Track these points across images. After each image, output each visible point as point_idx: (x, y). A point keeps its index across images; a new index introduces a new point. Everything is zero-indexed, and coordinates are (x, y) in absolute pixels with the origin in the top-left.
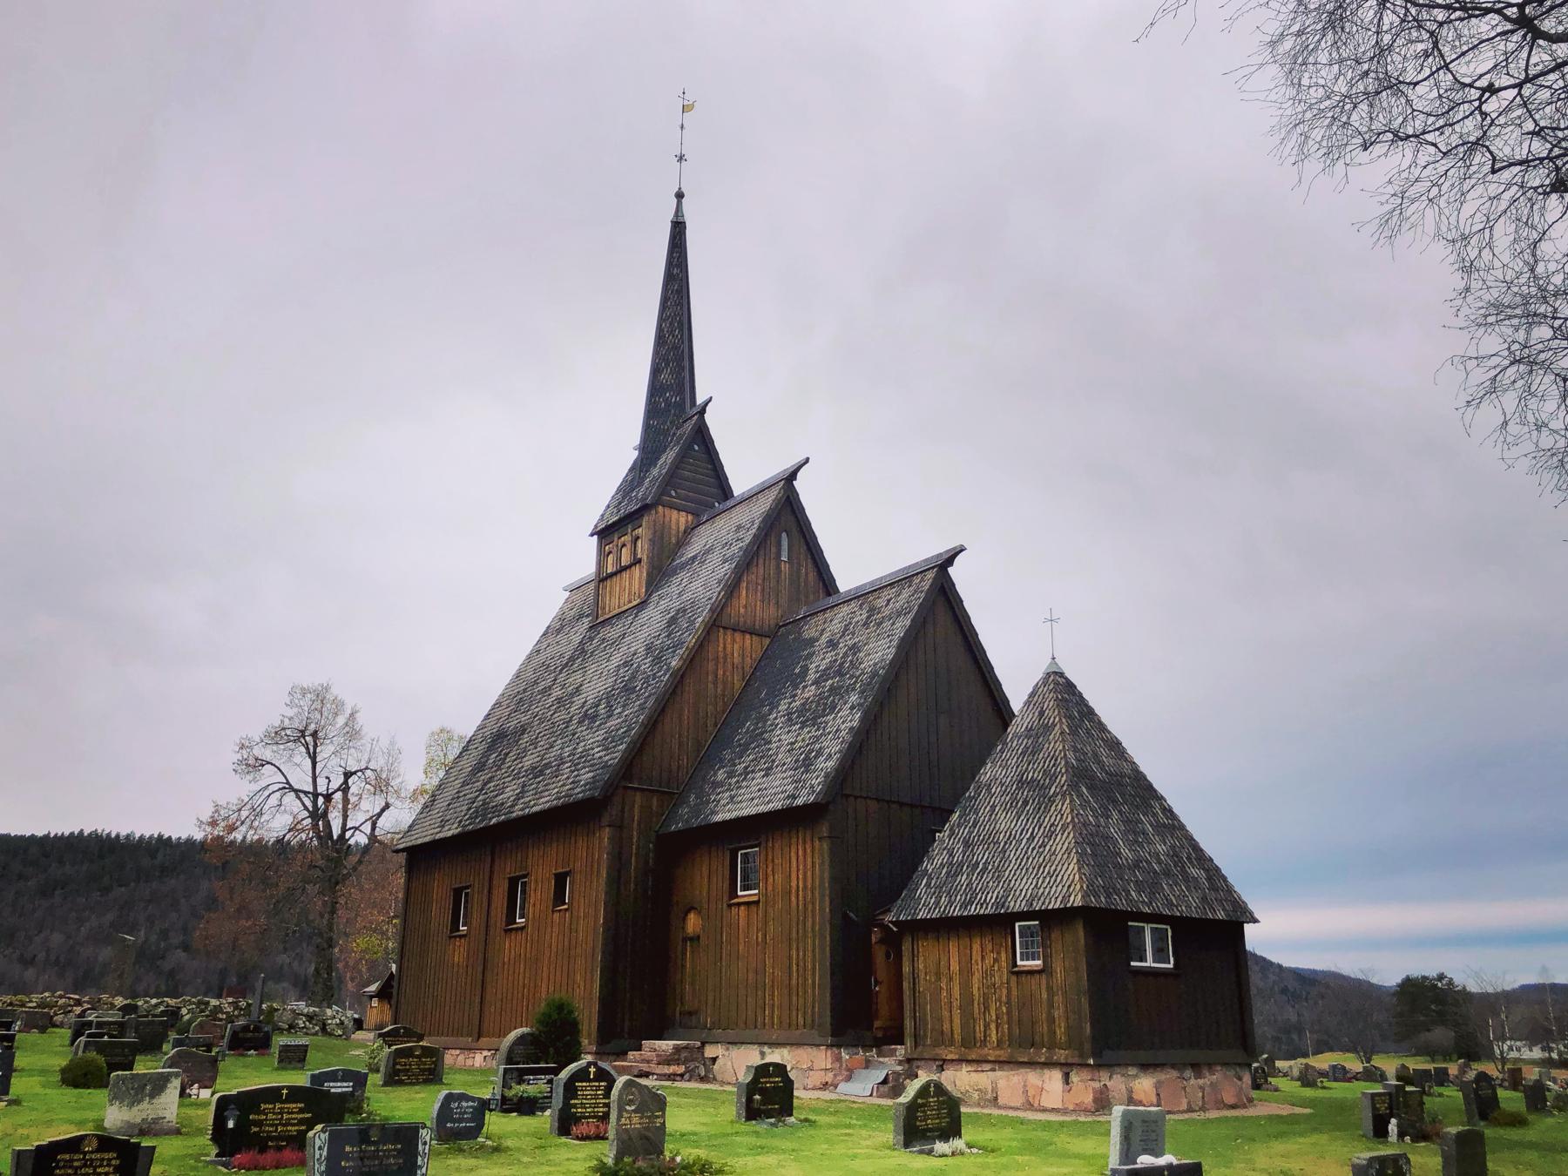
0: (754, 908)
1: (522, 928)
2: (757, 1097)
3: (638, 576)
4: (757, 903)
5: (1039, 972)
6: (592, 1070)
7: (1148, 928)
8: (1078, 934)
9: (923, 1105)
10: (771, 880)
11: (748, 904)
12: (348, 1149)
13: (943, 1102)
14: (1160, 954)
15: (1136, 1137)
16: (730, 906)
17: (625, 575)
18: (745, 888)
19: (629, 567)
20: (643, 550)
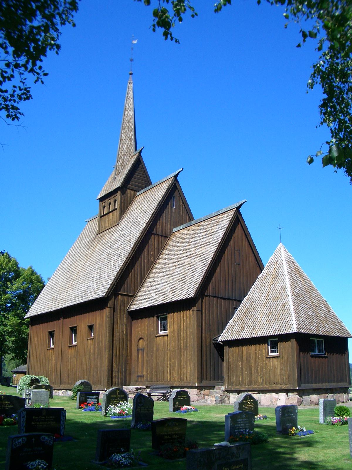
0: (166, 337)
1: (76, 346)
2: (177, 403)
3: (116, 214)
4: (167, 335)
5: (278, 357)
6: (118, 391)
7: (316, 340)
8: (293, 343)
9: (246, 403)
10: (172, 327)
11: (164, 336)
12: (34, 417)
13: (252, 402)
14: (319, 351)
15: (328, 409)
16: (156, 337)
17: (111, 214)
18: (162, 330)
19: (107, 214)
20: (117, 205)
